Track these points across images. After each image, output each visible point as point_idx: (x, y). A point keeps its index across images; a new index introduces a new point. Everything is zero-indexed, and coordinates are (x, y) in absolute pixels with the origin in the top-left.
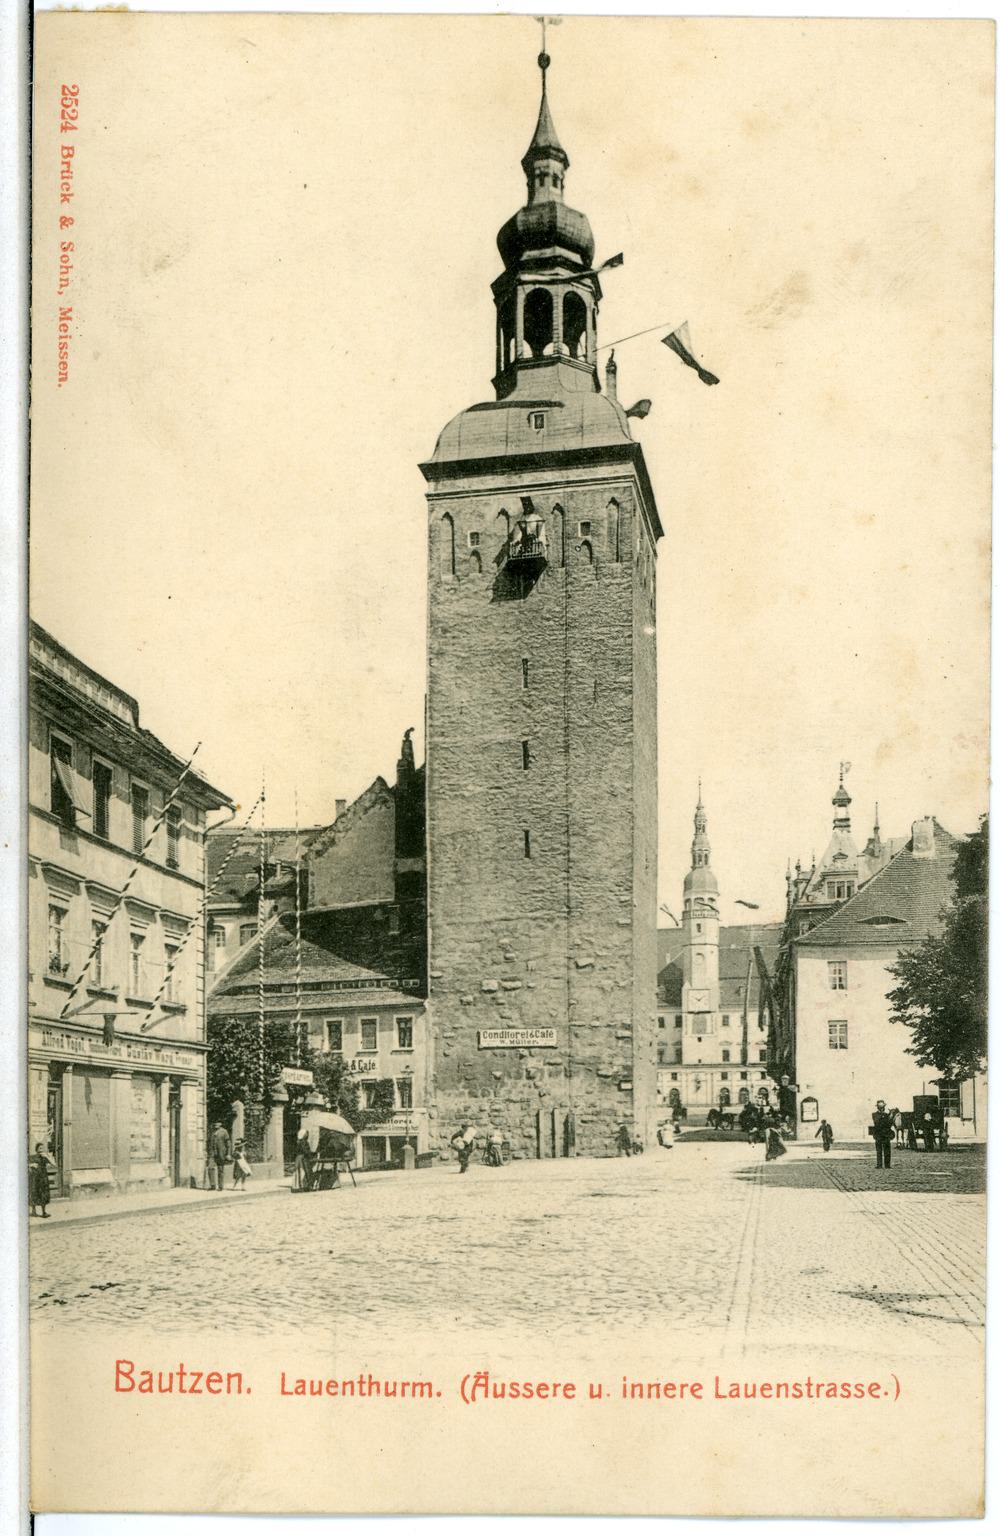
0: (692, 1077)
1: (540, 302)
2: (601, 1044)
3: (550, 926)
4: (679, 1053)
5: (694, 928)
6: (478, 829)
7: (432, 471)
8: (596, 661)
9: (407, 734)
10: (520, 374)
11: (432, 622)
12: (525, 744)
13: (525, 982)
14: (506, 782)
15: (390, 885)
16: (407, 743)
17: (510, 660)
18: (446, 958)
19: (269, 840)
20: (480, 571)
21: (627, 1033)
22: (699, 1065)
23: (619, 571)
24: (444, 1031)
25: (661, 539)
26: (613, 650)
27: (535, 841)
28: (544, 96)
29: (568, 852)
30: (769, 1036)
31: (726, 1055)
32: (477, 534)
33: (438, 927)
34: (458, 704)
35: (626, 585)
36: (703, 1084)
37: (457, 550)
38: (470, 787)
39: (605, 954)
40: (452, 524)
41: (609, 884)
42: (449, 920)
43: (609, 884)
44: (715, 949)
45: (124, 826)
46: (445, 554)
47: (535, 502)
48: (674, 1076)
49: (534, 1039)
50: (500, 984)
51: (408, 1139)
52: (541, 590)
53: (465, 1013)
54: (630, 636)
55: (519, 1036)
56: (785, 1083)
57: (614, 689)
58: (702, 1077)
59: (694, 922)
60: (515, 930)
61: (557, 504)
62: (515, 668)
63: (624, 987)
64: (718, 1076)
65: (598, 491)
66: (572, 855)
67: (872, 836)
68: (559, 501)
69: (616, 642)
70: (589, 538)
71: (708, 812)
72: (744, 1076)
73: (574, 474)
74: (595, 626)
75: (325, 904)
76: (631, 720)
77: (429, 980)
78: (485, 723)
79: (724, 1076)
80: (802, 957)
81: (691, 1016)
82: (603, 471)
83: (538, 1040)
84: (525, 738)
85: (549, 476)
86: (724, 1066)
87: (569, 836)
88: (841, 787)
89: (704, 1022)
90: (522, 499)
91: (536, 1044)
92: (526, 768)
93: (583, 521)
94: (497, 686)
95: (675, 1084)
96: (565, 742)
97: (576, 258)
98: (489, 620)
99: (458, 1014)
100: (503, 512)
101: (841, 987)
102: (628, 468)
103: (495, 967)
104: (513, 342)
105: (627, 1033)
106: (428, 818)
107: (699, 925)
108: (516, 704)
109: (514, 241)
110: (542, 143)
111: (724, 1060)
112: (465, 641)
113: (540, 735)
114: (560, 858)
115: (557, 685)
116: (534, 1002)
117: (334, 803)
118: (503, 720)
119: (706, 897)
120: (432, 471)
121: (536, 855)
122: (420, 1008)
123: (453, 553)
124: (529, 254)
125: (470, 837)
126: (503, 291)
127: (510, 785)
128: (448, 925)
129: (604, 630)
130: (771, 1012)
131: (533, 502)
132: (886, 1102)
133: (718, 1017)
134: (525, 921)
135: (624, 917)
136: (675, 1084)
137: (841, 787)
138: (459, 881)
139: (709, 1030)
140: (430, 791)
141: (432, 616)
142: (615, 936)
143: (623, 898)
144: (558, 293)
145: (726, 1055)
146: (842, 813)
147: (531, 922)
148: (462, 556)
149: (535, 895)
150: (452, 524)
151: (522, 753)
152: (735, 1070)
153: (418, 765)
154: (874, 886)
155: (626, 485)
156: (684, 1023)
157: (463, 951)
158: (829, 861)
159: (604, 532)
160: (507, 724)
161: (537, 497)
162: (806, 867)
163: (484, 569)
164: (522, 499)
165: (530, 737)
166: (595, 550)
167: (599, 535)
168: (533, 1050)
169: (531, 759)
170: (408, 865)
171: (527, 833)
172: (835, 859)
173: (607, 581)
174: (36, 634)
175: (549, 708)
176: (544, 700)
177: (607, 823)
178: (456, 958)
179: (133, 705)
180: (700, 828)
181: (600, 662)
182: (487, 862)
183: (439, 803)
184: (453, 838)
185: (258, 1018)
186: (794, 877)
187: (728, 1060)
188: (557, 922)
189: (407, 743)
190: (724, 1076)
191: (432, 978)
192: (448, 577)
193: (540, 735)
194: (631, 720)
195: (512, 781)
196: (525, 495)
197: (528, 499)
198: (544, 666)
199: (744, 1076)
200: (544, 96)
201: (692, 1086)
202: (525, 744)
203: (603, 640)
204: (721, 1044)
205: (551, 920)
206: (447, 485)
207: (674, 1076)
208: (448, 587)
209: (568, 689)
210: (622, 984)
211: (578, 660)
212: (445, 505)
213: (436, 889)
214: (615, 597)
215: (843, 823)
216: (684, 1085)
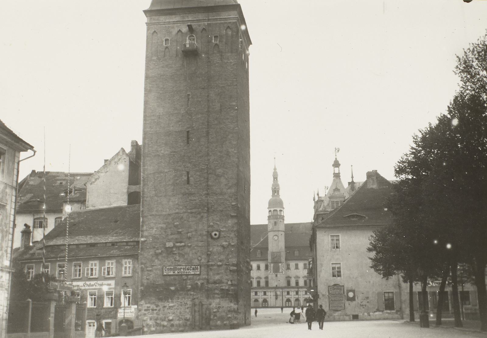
2: (222, 273)
3: (199, 216)
4: (267, 283)
6: (166, 171)
12: (188, 132)
13: (186, 243)
15: (126, 197)
18: (149, 232)
19: (72, 178)
22: (277, 288)
24: (147, 267)
27: (192, 176)
30: (307, 274)
31: (289, 283)
33: (146, 217)
34: (158, 114)
35: (234, 63)
39: (225, 230)
41: (226, 197)
43: (226, 197)
44: (283, 233)
47: (194, 27)
48: (265, 294)
49: (189, 271)
50: (174, 244)
51: (124, 321)
53: (157, 258)
54: (236, 85)
55: (182, 270)
58: (278, 293)
60: (182, 218)
65: (222, 23)
66: (210, 183)
72: (297, 293)
75: (94, 207)
83: (191, 271)
87: (208, 174)
88: (336, 158)
90: (188, 26)
91: (190, 273)
93: (215, 35)
95: (265, 297)
99: (154, 259)
100: (180, 31)
101: (337, 247)
103: (172, 236)
106: (142, 166)
116: (191, 252)
119: (278, 209)
121: (192, 183)
128: (150, 216)
131: (193, 27)
132: (340, 149)
134: (187, 214)
136: (265, 297)
137: (336, 158)
138: (156, 195)
142: (229, 221)
147: (190, 215)
149: (192, 202)
152: (293, 290)
155: (234, 21)
156: (269, 268)
157: (157, 228)
164: (188, 26)
168: (189, 276)
170: (134, 188)
172: (334, 190)
173: (226, 61)
177: (226, 168)
178: (154, 231)
180: (275, 178)
182: (170, 186)
183: (147, 158)
185: (79, 267)
187: (290, 285)
188: (202, 214)
196: (189, 24)
197: (191, 25)
199: (297, 293)
202: (188, 132)
203: (224, 87)
205: (199, 213)
207: (265, 294)
210: (232, 244)
213: (145, 199)
215: (337, 176)
216: (269, 297)
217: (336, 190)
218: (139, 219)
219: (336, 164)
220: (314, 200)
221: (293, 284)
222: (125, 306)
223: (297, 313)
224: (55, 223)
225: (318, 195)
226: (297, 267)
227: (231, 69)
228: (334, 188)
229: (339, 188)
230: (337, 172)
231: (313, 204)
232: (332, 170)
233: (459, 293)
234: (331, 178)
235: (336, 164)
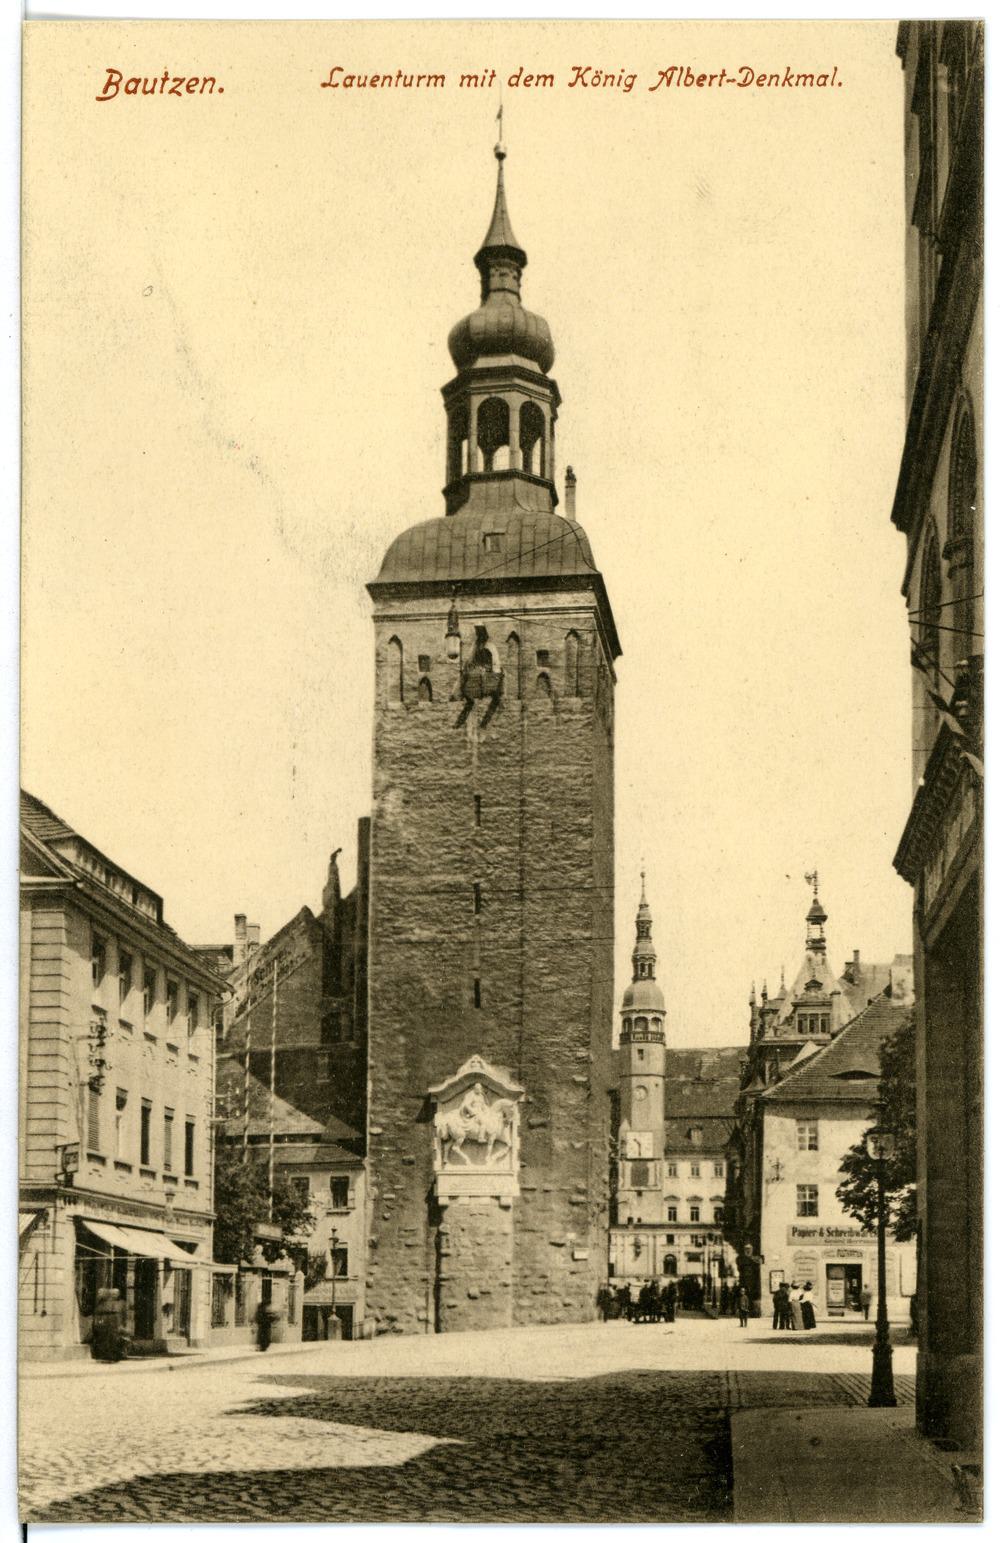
0: (631, 1240)
1: (495, 414)
5: (635, 1055)
7: (376, 590)
8: (553, 801)
9: (334, 857)
10: (475, 487)
11: (377, 752)
14: (456, 927)
16: (334, 871)
17: (461, 796)
20: (431, 700)
21: (582, 1198)
23: (579, 706)
25: (619, 658)
26: (572, 790)
28: (500, 186)
29: (521, 1003)
31: (673, 1214)
32: (427, 658)
36: (643, 1249)
37: (406, 677)
38: (417, 931)
40: (401, 648)
42: (392, 1073)
44: (660, 1081)
45: (872, 1270)
46: (392, 680)
52: (496, 723)
56: (750, 1254)
57: (573, 832)
58: (643, 1239)
59: (635, 1047)
61: (513, 633)
62: (467, 804)
63: (578, 1150)
64: (663, 1240)
67: (852, 960)
68: (515, 630)
69: (574, 782)
70: (547, 670)
71: (653, 912)
73: (531, 601)
74: (552, 763)
76: (591, 865)
77: (368, 1137)
78: (434, 863)
79: (670, 1239)
80: (769, 1114)
81: (629, 1165)
82: (563, 599)
84: (476, 881)
85: (505, 602)
86: (670, 1227)
88: (815, 901)
89: (646, 1171)
90: (477, 628)
92: (478, 911)
94: (448, 824)
96: (521, 886)
97: (534, 367)
98: (440, 752)
102: (587, 598)
104: (465, 444)
105: (582, 1198)
107: (641, 1051)
108: (468, 843)
109: (466, 344)
110: (496, 242)
111: (692, 1219)
112: (413, 774)
113: (493, 877)
114: (513, 1009)
115: (512, 825)
117: (233, 920)
118: (455, 861)
120: (376, 590)
122: (358, 1167)
123: (401, 678)
124: (482, 363)
125: (415, 984)
126: (455, 395)
127: (460, 930)
129: (563, 768)
130: (936, 212)
133: (665, 1166)
135: (581, 1074)
137: (815, 901)
139: (651, 1180)
140: (373, 934)
141: (378, 745)
143: (579, 1054)
144: (515, 401)
145: (673, 1214)
146: (816, 934)
148: (411, 683)
150: (401, 648)
151: (474, 897)
153: (344, 894)
154: (848, 1035)
158: (801, 990)
159: (562, 663)
160: (457, 865)
161: (490, 623)
162: (773, 995)
163: (434, 698)
165: (482, 880)
166: (554, 682)
167: (557, 667)
169: (482, 903)
171: (477, 982)
172: (808, 987)
174: (31, 805)
175: (502, 849)
176: (497, 840)
179: (157, 902)
181: (557, 802)
184: (398, 986)
186: (759, 1003)
189: (334, 871)
190: (670, 1239)
191: (372, 1134)
192: (396, 705)
193: (493, 877)
194: (591, 865)
195: (462, 925)
198: (498, 804)
200: (500, 186)
201: (630, 1250)
204: (666, 1199)
206: (397, 608)
208: (395, 715)
209: (523, 831)
211: (535, 804)
212: (390, 630)
214: (574, 734)
215: (817, 945)
217: (814, 985)
218: (364, 1088)
219: (817, 917)
220: (752, 1004)
221: (684, 1215)
222: (890, 1318)
223: (894, 1356)
224: (378, 684)
225: (764, 995)
226: (696, 1173)
227: (425, 976)
228: (808, 980)
229: (819, 980)
230: (816, 935)
231: (747, 1014)
232: (805, 931)
233: (347, 1174)
234: (802, 952)
235: (817, 917)
